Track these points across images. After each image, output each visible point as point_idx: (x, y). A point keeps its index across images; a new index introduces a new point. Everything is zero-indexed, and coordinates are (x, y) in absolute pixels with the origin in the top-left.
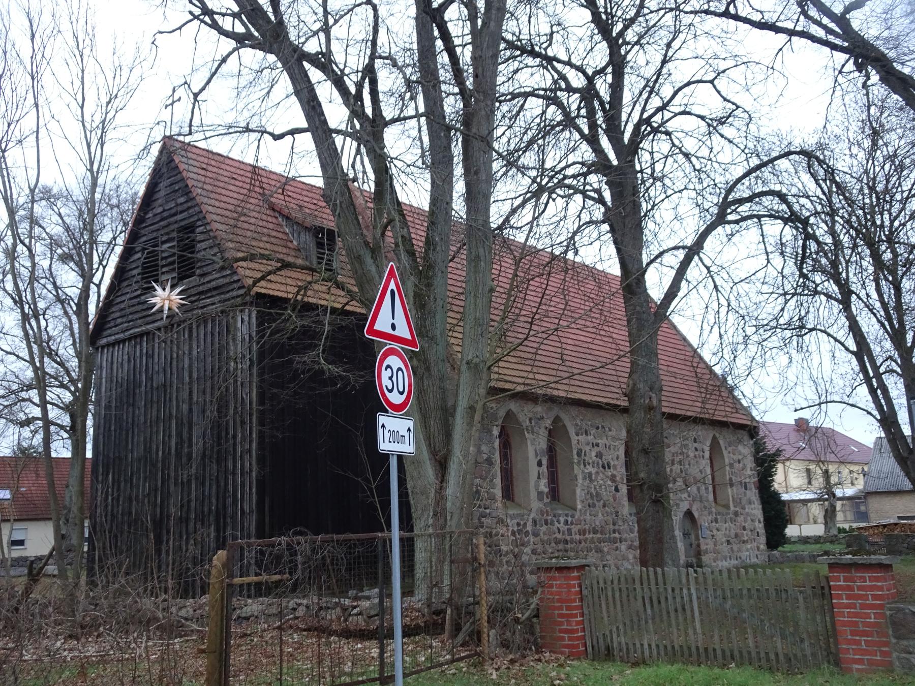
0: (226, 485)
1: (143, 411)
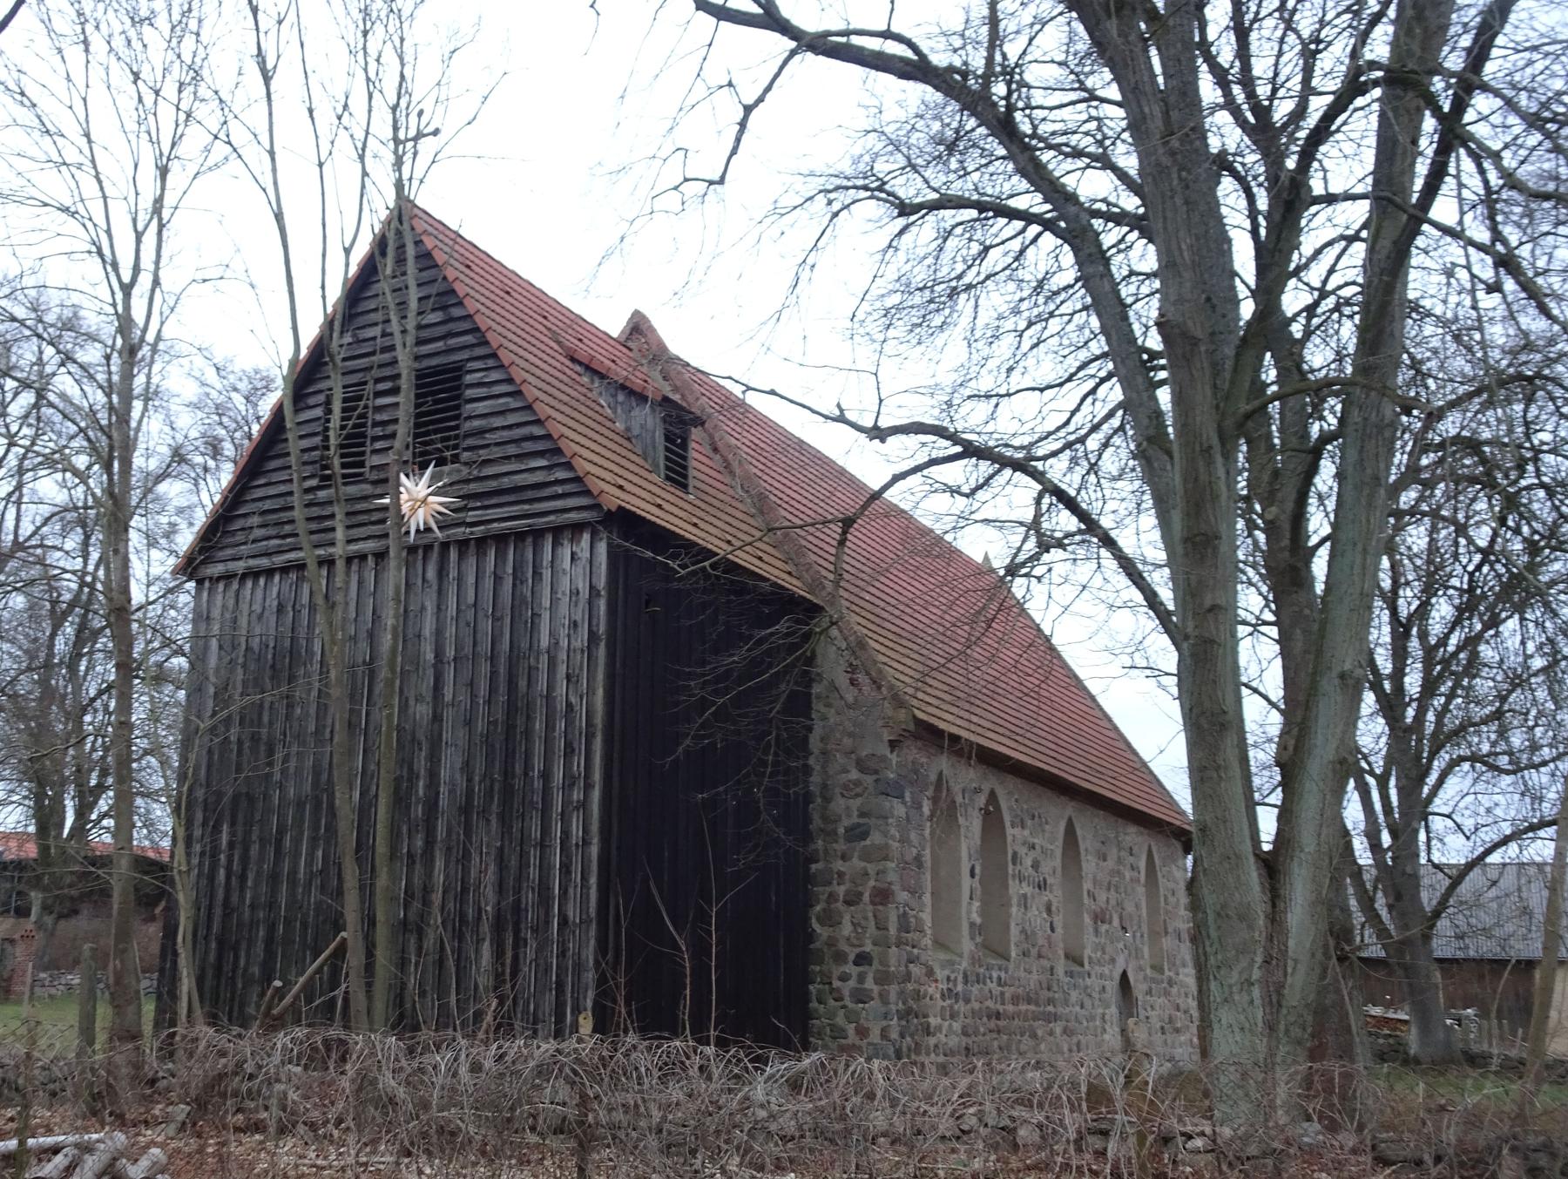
0: (523, 865)
1: (313, 710)
